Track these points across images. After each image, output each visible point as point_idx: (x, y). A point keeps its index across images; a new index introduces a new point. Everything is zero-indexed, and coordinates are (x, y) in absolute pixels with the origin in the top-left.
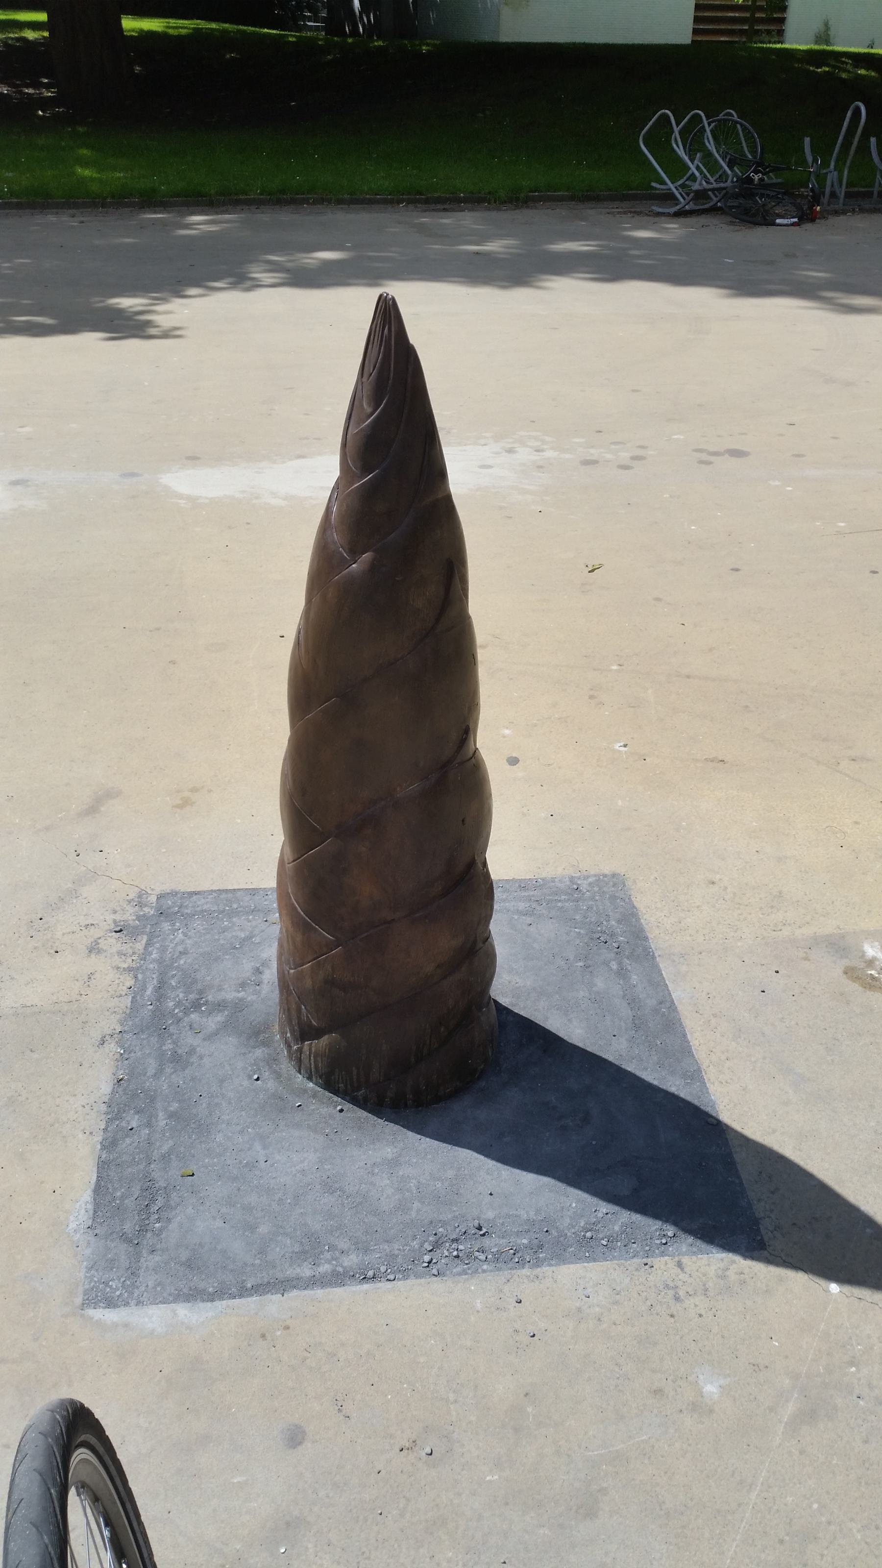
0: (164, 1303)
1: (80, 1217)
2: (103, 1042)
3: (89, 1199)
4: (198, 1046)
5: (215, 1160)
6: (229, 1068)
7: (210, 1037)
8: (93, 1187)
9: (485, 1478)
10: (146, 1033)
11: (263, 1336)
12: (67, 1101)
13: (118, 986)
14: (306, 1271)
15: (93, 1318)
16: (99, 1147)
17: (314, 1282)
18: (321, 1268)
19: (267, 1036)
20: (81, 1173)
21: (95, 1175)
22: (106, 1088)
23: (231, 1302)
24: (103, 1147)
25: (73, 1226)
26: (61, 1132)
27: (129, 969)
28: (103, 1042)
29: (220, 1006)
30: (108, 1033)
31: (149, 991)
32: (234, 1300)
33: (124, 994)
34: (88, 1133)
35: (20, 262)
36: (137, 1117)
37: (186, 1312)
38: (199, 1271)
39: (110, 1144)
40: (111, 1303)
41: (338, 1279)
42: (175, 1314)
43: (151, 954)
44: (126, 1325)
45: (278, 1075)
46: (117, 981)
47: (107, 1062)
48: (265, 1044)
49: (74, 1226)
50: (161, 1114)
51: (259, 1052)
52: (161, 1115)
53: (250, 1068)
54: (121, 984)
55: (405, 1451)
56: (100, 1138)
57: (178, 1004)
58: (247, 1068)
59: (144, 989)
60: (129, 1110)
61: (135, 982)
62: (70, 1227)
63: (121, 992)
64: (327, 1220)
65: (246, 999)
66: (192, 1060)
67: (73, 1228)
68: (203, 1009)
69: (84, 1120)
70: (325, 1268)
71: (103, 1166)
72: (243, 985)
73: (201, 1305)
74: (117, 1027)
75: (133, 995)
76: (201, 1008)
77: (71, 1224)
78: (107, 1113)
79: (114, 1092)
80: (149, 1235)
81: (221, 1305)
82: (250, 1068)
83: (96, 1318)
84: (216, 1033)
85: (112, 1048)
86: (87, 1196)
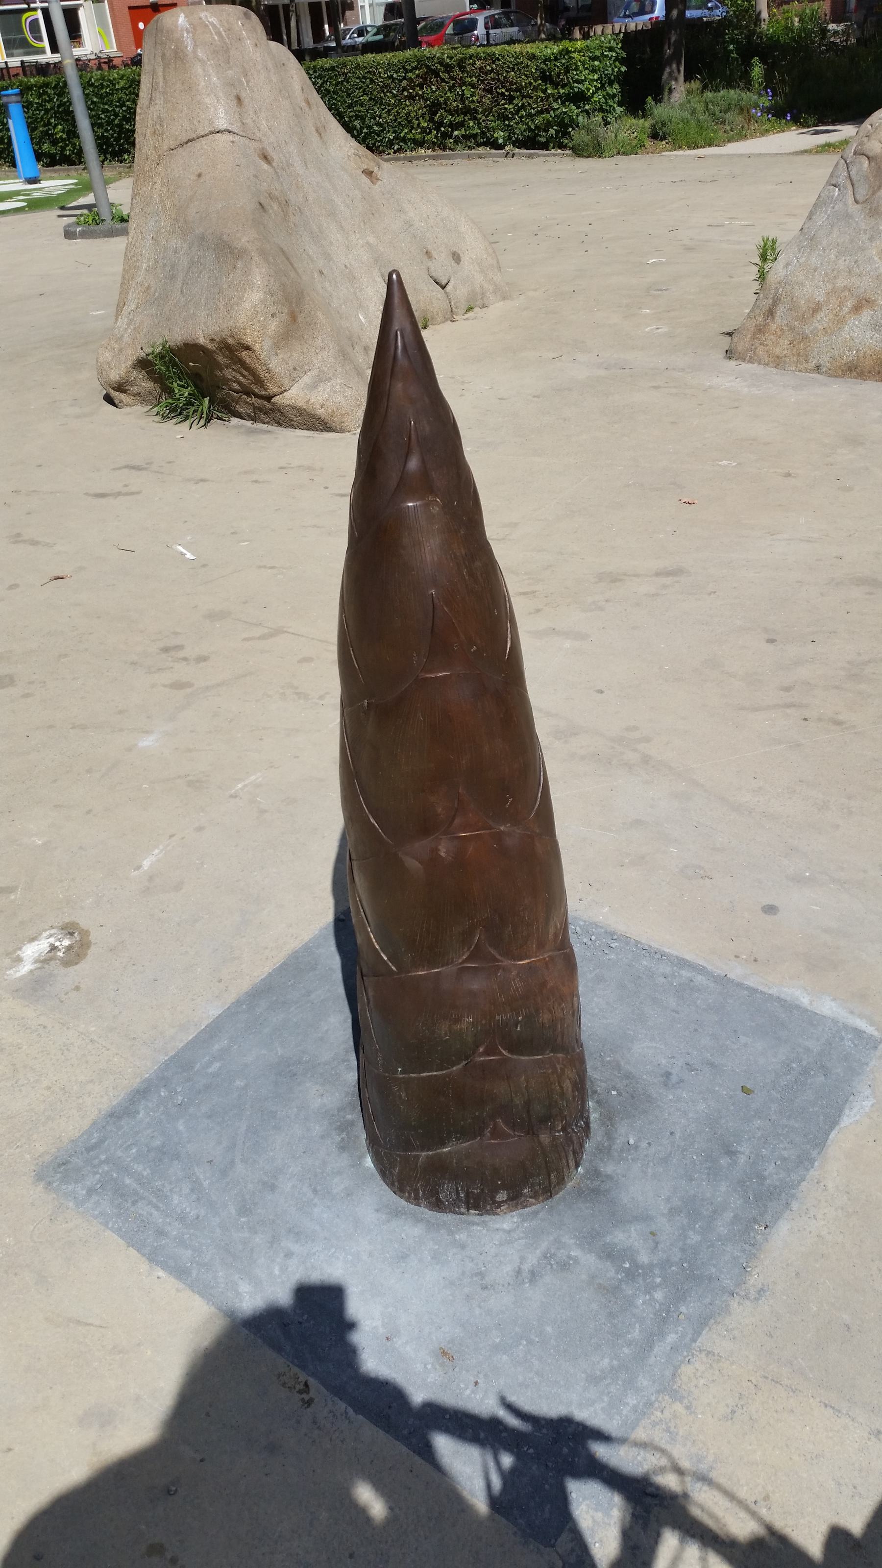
0: (816, 1013)
1: (859, 1107)
2: (761, 1291)
3: (845, 1118)
4: (663, 1215)
5: (717, 1089)
6: (649, 1170)
7: (645, 1218)
8: (837, 1128)
9: (763, 61)
10: (707, 1273)
11: (755, 960)
12: (829, 1233)
13: (703, 1372)
14: (700, 979)
15: (876, 1029)
16: (816, 1164)
17: (702, 970)
18: (688, 975)
19: (588, 1182)
20: (844, 1145)
21: (830, 1137)
22: (783, 1228)
23: (766, 990)
24: (812, 1161)
25: (868, 1104)
26: (849, 1199)
27: (676, 1396)
28: (761, 1291)
29: (610, 1254)
30: (748, 1303)
31: (671, 1338)
32: (763, 990)
33: (703, 1355)
34: (822, 1184)
35: (401, 352)
36: (766, 1173)
37: (802, 999)
38: (783, 285)
39: (805, 1161)
40: (858, 1033)
41: (683, 963)
42: (811, 1002)
43: (635, 1409)
44: (852, 1013)
45: (609, 1136)
46: (702, 1382)
47: (768, 1262)
48: (595, 1174)
49: (867, 1102)
50: (742, 1161)
51: (608, 1168)
52: (742, 1159)
53: (629, 1157)
54: (699, 1374)
55: (710, 877)
56: (812, 1172)
57: (649, 1289)
58: (632, 1159)
59: (674, 1349)
60: (769, 1186)
61: (679, 1366)
62: (871, 1103)
63: (705, 1359)
64: (661, 999)
65: (575, 1243)
66: (679, 1203)
67: (869, 1101)
68: (627, 1265)
69: (820, 1201)
70: (686, 973)
71: (820, 1142)
72: (564, 1266)
73: (788, 999)
74: (736, 1305)
75: (694, 1345)
76: (629, 1269)
77: (869, 1105)
78: (793, 1196)
79: (777, 1218)
80: (804, 1063)
81: (774, 991)
82: (629, 1157)
83: (874, 1028)
84: (636, 1219)
85: (754, 1280)
86: (845, 1121)
